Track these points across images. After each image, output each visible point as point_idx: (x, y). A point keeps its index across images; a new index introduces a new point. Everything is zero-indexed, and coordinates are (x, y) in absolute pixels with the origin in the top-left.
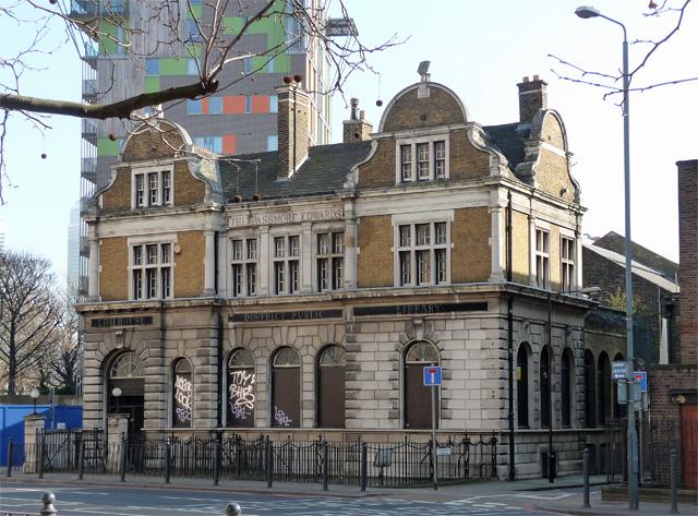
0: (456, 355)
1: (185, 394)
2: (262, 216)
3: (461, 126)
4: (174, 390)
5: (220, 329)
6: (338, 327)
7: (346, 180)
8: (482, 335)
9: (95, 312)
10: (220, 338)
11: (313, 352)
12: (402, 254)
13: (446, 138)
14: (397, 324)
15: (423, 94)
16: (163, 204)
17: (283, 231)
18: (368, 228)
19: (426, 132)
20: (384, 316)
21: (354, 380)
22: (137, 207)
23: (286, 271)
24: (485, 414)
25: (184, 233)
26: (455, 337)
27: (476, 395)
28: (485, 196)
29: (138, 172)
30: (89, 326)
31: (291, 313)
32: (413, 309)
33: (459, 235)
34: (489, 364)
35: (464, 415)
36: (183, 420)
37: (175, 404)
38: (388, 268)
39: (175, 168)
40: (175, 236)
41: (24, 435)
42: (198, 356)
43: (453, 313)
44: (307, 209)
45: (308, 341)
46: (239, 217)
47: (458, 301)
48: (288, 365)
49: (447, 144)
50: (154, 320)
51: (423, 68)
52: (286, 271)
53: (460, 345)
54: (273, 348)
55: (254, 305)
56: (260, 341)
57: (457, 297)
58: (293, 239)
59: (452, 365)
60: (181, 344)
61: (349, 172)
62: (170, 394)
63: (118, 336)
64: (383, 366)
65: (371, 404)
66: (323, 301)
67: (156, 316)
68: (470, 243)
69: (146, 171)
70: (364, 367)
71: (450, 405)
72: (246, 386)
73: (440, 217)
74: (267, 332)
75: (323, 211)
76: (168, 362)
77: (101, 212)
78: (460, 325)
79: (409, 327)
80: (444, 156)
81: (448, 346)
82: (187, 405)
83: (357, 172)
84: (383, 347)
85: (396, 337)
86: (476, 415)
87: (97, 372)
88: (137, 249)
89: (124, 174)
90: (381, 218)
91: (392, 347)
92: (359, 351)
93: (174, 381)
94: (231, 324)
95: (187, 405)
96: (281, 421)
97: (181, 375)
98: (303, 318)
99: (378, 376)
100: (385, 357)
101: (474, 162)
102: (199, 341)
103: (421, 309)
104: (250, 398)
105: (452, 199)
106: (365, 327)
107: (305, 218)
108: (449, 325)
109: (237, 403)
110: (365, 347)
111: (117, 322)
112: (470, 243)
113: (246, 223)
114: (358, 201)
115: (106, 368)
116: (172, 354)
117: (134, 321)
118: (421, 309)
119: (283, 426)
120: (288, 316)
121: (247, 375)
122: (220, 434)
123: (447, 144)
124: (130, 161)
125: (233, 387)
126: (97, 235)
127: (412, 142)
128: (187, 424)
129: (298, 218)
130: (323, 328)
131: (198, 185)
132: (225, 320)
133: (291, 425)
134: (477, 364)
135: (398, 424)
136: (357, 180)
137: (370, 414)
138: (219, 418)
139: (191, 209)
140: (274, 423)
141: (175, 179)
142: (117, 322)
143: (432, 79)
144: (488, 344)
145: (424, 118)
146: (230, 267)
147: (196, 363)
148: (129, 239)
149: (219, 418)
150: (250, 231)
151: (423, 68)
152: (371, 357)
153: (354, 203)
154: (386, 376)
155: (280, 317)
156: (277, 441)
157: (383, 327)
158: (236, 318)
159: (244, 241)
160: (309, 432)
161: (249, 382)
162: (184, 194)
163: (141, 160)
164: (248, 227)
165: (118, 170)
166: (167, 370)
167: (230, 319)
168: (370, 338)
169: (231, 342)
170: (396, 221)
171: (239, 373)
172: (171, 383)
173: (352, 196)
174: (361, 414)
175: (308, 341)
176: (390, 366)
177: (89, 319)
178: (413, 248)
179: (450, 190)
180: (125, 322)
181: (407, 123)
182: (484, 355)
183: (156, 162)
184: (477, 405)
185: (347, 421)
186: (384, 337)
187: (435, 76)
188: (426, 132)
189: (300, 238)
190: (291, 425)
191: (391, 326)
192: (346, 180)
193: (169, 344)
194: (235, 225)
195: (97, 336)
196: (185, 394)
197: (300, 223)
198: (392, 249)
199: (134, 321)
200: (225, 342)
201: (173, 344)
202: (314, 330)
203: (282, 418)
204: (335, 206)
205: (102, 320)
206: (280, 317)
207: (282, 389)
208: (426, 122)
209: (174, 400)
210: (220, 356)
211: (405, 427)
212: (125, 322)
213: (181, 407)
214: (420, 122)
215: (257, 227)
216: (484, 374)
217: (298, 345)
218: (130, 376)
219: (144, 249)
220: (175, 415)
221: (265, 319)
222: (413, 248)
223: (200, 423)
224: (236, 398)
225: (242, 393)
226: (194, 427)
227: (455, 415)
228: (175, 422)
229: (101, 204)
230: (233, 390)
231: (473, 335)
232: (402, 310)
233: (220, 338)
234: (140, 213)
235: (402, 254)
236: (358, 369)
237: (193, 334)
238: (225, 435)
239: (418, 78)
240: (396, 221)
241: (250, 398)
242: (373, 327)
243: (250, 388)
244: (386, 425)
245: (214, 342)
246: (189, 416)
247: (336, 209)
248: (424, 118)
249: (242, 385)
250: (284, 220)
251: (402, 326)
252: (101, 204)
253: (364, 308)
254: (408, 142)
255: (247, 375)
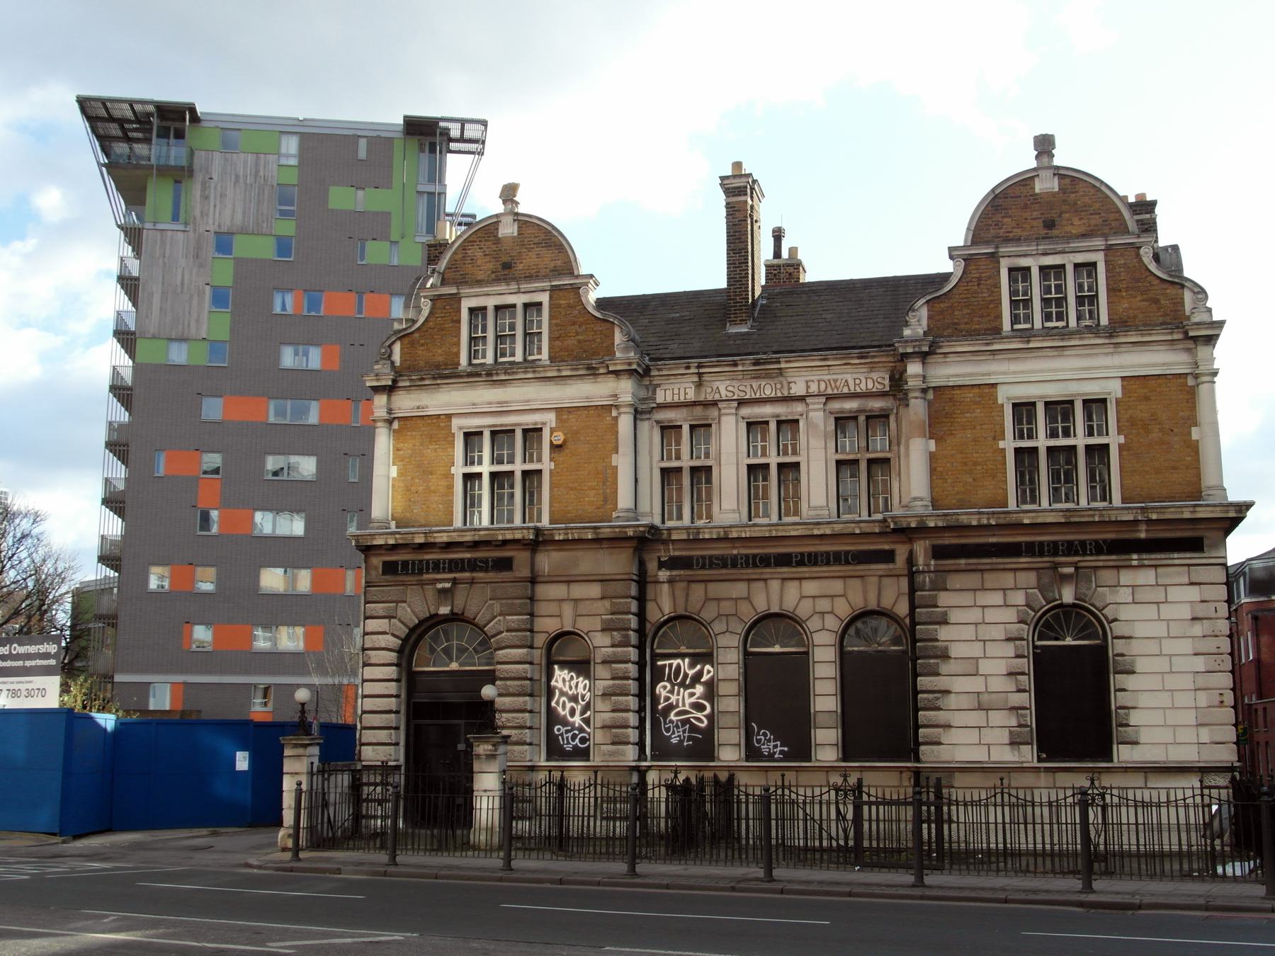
0: (1140, 630)
1: (574, 699)
2: (723, 387)
3: (567, 281)
4: (550, 692)
5: (643, 581)
6: (886, 581)
7: (907, 324)
8: (1194, 593)
9: (394, 547)
10: (642, 599)
11: (833, 623)
12: (468, 478)
13: (544, 298)
14: (1019, 574)
15: (1046, 185)
16: (525, 360)
17: (766, 411)
18: (946, 407)
19: (1059, 247)
20: (995, 560)
21: (939, 709)
22: (470, 364)
23: (773, 478)
24: (1205, 735)
25: (570, 410)
26: (1139, 598)
27: (1185, 699)
28: (1183, 357)
29: (474, 303)
30: (377, 574)
31: (789, 555)
32: (1054, 549)
33: (1133, 422)
34: (1211, 645)
35: (1165, 736)
36: (568, 748)
37: (552, 718)
38: (994, 476)
39: (551, 297)
40: (551, 418)
41: (282, 774)
42: (603, 630)
43: (1135, 556)
44: (815, 376)
45: (824, 605)
46: (677, 388)
47: (1143, 535)
48: (777, 649)
49: (1101, 268)
50: (515, 563)
51: (1044, 145)
52: (773, 478)
53: (1151, 611)
54: (750, 617)
55: (718, 539)
56: (723, 604)
57: (1143, 527)
58: (788, 425)
59: (1135, 647)
60: (568, 610)
61: (911, 309)
62: (544, 700)
63: (444, 591)
64: (993, 650)
65: (975, 718)
66: (862, 534)
67: (521, 557)
68: (1155, 435)
69: (491, 302)
70: (956, 651)
71: (1135, 718)
72: (692, 686)
73: (1092, 389)
74: (739, 589)
75: (850, 378)
76: (540, 640)
77: (398, 373)
78: (1147, 576)
79: (1046, 580)
80: (539, 327)
81: (1125, 613)
82: (577, 720)
83: (924, 312)
84: (991, 615)
85: (1019, 598)
86: (1188, 735)
87: (392, 657)
88: (471, 437)
89: (446, 306)
90: (976, 390)
91: (1011, 615)
92: (944, 622)
93: (550, 675)
94: (664, 574)
95: (577, 720)
96: (765, 749)
97: (564, 664)
98: (815, 564)
99: (985, 667)
100: (998, 632)
101: (1156, 301)
102: (607, 603)
103: (1071, 548)
104: (699, 707)
105: (1117, 360)
106: (955, 581)
107: (814, 388)
108: (1126, 577)
109: (672, 717)
110: (954, 616)
111: (437, 566)
112: (1155, 435)
113: (691, 395)
114: (931, 359)
115: (407, 650)
116: (548, 625)
117: (473, 566)
118: (1071, 548)
119: (771, 757)
120: (784, 560)
121: (692, 666)
122: (642, 773)
123: (1101, 268)
124: (458, 284)
125: (662, 689)
126: (390, 411)
127: (1033, 263)
128: (583, 754)
129: (798, 389)
130: (856, 583)
131: (599, 327)
132: (652, 566)
133: (787, 757)
134: (1186, 646)
135: (1028, 755)
136: (925, 322)
137: (973, 736)
138: (641, 744)
139: (589, 368)
140: (752, 753)
141: (551, 317)
142: (437, 566)
143: (1057, 161)
144: (1208, 610)
145: (1050, 225)
146: (744, 471)
147: (601, 643)
148: (456, 422)
149: (641, 744)
150: (698, 411)
151: (1044, 145)
152: (969, 632)
153: (389, 396)
154: (1002, 667)
155: (765, 561)
156: (751, 783)
157: (991, 579)
158: (673, 563)
159: (686, 429)
160: (829, 769)
161: (697, 678)
162: (571, 342)
163: (479, 283)
164: (694, 404)
165: (435, 299)
166: (538, 655)
167: (662, 565)
168: (966, 599)
169: (664, 603)
170: (1006, 396)
171: (675, 662)
172: (544, 679)
173: (926, 349)
174: (946, 737)
175: (824, 605)
176: (1009, 650)
177: (377, 561)
178: (1080, 440)
179: (994, 352)
180: (455, 566)
181: (1018, 232)
182: (1197, 629)
183: (514, 286)
184: (1190, 717)
185: (922, 748)
186: (997, 598)
187: (527, 205)
188: (1059, 247)
189: (801, 424)
190: (787, 757)
191: (1008, 579)
192: (907, 324)
193: (541, 608)
194: (669, 400)
195: (394, 592)
196: (574, 699)
197: (802, 399)
198: (1001, 444)
199: (473, 566)
200: (651, 607)
201: (552, 608)
202: (836, 586)
203: (770, 745)
204: (872, 370)
205: (405, 563)
206: (765, 561)
207: (774, 695)
208: (1055, 232)
209: (551, 712)
210: (641, 631)
211: (1040, 760)
212: (455, 566)
213: (564, 722)
214: (1043, 232)
215: (714, 403)
216: (1200, 664)
217: (707, 615)
218: (454, 666)
219: (1040, 409)
220: (552, 741)
221: (734, 565)
222: (1042, 442)
223: (612, 754)
224: (670, 707)
225: (681, 700)
226: (596, 760)
227: (1144, 736)
228: (554, 750)
229: (397, 357)
230: (664, 693)
231: (1174, 593)
232: (1031, 549)
233: (642, 599)
234: (478, 375)
235: (468, 478)
236: (945, 656)
237: (595, 590)
238: (652, 777)
239: (498, 207)
240: (1006, 396)
241: (699, 707)
242: (972, 580)
243: (699, 689)
244: (1005, 755)
245: (634, 606)
246: (583, 740)
247: (875, 375)
248: (1050, 225)
249: (682, 685)
250: (768, 392)
251: (1030, 578)
252: (397, 357)
253: (994, 545)
254: (1024, 262)
255: (692, 666)
